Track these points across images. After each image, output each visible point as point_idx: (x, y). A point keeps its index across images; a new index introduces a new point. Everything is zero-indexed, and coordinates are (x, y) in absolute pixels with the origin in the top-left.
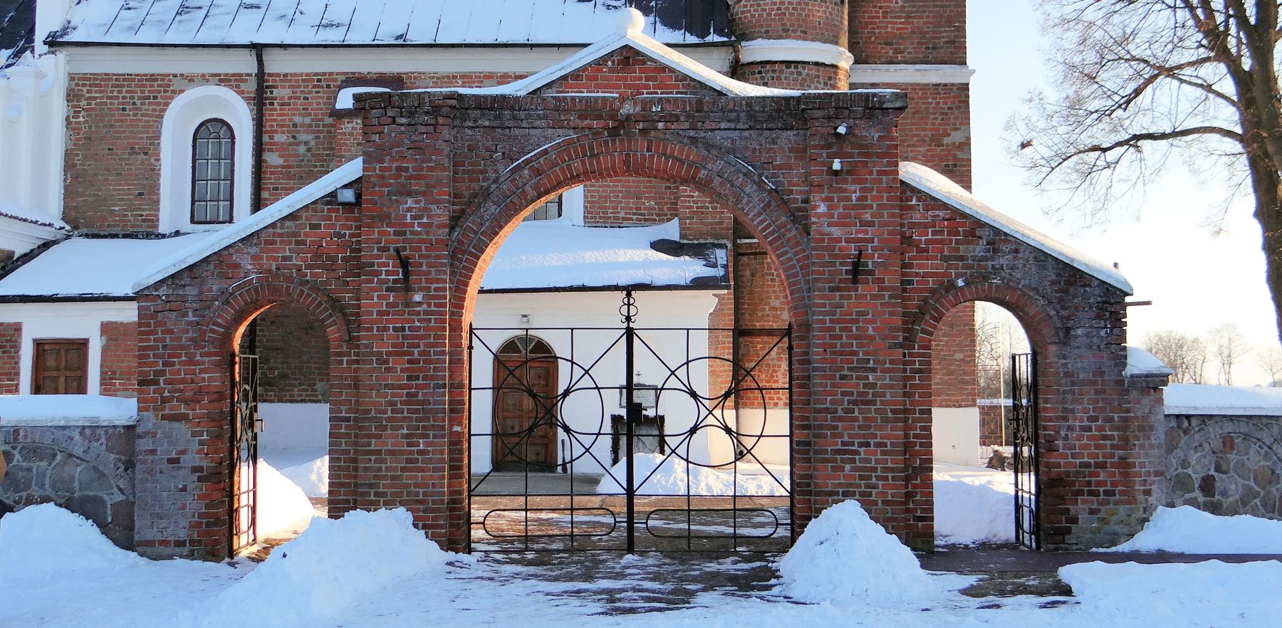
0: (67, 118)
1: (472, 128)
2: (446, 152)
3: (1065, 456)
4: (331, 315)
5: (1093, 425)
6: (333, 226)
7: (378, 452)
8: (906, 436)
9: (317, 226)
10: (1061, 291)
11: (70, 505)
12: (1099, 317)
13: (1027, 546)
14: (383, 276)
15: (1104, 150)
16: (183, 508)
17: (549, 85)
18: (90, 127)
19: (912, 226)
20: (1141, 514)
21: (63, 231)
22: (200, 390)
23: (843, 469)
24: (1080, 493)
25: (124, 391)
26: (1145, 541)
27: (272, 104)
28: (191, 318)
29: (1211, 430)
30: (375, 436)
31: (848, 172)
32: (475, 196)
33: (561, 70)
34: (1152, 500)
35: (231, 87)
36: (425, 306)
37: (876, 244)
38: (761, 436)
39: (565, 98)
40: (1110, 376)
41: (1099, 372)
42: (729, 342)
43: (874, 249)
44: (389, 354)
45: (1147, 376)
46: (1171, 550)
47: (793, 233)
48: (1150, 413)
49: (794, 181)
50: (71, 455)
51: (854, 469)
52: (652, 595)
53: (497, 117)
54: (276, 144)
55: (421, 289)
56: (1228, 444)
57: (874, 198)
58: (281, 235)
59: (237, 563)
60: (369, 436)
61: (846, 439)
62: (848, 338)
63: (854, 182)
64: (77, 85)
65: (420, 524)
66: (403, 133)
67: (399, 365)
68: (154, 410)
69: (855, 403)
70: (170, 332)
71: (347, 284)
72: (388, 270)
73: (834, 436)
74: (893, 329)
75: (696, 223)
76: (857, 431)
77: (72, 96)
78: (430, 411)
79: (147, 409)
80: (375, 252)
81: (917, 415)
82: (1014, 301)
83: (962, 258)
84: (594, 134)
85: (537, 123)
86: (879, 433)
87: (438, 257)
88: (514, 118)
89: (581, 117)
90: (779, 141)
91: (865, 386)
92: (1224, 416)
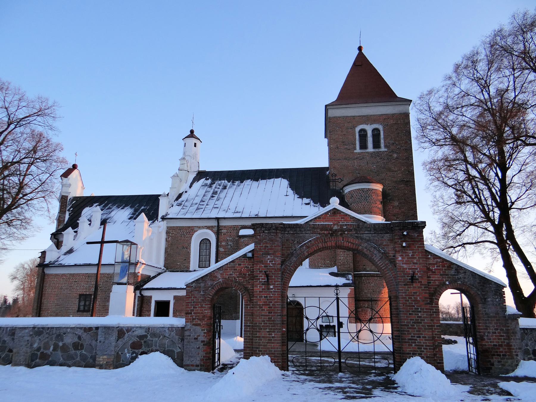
0: (166, 239)
1: (287, 234)
2: (280, 241)
4: (244, 292)
5: (497, 331)
7: (259, 337)
8: (433, 334)
9: (240, 265)
11: (164, 352)
12: (495, 295)
13: (474, 373)
14: (261, 280)
15: (455, 248)
16: (199, 354)
17: (311, 221)
18: (172, 241)
19: (430, 264)
20: (516, 363)
21: (164, 270)
22: (204, 316)
24: (494, 355)
25: (182, 317)
26: (519, 372)
27: (221, 234)
28: (202, 293)
29: (534, 333)
31: (408, 247)
32: (289, 255)
33: (314, 216)
35: (210, 230)
36: (274, 290)
37: (418, 270)
38: (382, 333)
41: (497, 313)
42: (353, 303)
43: (417, 271)
44: (262, 305)
46: (530, 376)
47: (390, 266)
48: (515, 327)
49: (390, 250)
50: (165, 336)
51: (415, 345)
52: (356, 390)
53: (296, 230)
54: (222, 245)
55: (272, 284)
57: (417, 255)
58: (229, 267)
59: (215, 372)
60: (256, 332)
61: (412, 335)
62: (411, 301)
63: (410, 250)
64: (169, 230)
65: (273, 361)
66: (266, 235)
67: (266, 308)
68: (190, 322)
69: (415, 323)
70: (196, 297)
71: (249, 282)
72: (262, 278)
73: (408, 334)
74: (426, 298)
76: (416, 332)
77: (167, 233)
78: (276, 324)
79: (188, 322)
80: (258, 272)
81: (436, 327)
82: (465, 289)
83: (447, 275)
84: (325, 235)
86: (423, 333)
87: (278, 274)
88: (300, 231)
89: (321, 230)
90: (384, 237)
91: (418, 317)
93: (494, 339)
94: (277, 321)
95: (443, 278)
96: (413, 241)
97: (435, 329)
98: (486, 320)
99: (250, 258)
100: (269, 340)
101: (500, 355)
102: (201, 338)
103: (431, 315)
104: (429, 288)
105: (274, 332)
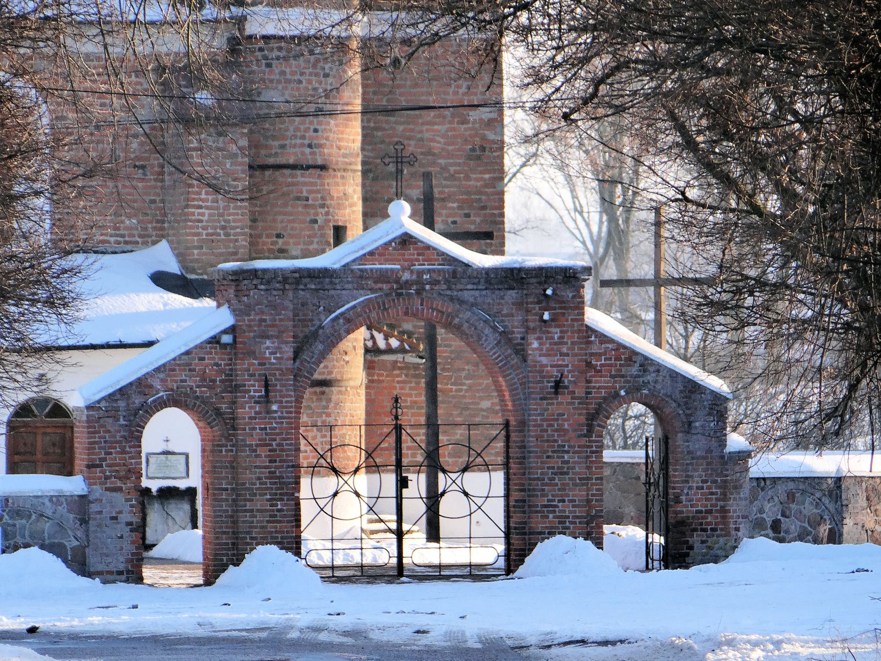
1: (303, 290)
3: (687, 506)
4: (215, 420)
5: (705, 485)
6: (214, 359)
7: (252, 511)
8: (588, 495)
9: (202, 359)
10: (686, 397)
12: (710, 414)
19: (592, 354)
20: (732, 543)
23: (548, 517)
24: (695, 530)
28: (122, 422)
30: (249, 500)
32: (306, 337)
33: (631, 457)
34: (739, 534)
36: (279, 413)
37: (570, 368)
38: (487, 497)
39: (366, 270)
40: (716, 454)
43: (569, 372)
44: (257, 445)
45: (739, 452)
50: (42, 515)
51: (554, 517)
56: (791, 497)
57: (569, 338)
58: (179, 365)
60: (246, 500)
61: (550, 497)
62: (552, 431)
67: (263, 452)
68: (100, 484)
69: (556, 474)
70: (109, 431)
71: (223, 398)
72: (255, 389)
73: (543, 496)
75: (206, 254)
76: (557, 492)
83: (623, 376)
85: (346, 286)
87: (288, 380)
88: (331, 282)
91: (563, 462)
92: (789, 478)
93: (698, 500)
94: (288, 477)
95: (615, 382)
96: (561, 308)
97: (592, 484)
98: (687, 464)
99: (225, 346)
100: (271, 516)
101: (705, 530)
102: (126, 517)
103: (588, 457)
104: (587, 404)
105: (282, 500)
